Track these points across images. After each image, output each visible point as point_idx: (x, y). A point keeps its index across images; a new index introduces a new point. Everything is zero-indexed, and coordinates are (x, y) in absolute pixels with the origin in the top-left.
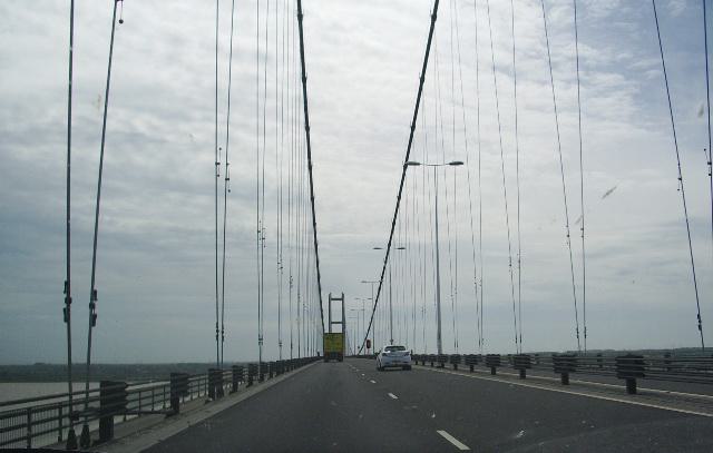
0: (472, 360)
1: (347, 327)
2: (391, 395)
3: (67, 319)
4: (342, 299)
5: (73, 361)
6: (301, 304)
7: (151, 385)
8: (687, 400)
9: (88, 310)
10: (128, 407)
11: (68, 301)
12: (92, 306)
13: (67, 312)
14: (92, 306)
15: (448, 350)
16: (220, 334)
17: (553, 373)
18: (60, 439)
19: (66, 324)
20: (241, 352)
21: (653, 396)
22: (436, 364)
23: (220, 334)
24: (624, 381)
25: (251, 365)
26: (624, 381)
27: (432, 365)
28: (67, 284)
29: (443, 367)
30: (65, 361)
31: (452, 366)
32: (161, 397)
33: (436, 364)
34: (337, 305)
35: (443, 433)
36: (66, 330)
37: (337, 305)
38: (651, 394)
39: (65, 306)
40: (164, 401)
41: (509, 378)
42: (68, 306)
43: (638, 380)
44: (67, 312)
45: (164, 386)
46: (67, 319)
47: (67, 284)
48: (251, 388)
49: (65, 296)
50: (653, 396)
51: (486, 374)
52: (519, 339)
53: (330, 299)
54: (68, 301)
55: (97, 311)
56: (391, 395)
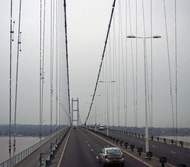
4: (77, 101)
34: (75, 103)
37: (75, 103)
53: (73, 101)
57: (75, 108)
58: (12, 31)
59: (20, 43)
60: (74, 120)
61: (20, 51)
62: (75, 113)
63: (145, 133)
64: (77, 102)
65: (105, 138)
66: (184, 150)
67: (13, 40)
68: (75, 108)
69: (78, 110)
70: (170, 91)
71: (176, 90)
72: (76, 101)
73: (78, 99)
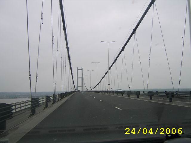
0: (117, 92)
3: (30, 80)
4: (82, 70)
6: (63, 61)
8: (142, 98)
10: (39, 103)
11: (30, 75)
12: (37, 77)
13: (30, 78)
14: (37, 77)
16: (54, 83)
17: (147, 96)
20: (60, 90)
21: (176, 103)
22: (102, 93)
23: (54, 83)
24: (149, 97)
25: (112, 91)
26: (149, 97)
28: (30, 72)
29: (110, 94)
31: (121, 95)
32: (17, 106)
34: (80, 72)
35: (120, 109)
36: (30, 81)
37: (80, 72)
40: (44, 100)
41: (120, 95)
43: (152, 97)
44: (30, 78)
45: (25, 102)
46: (30, 80)
47: (30, 72)
48: (34, 117)
50: (176, 103)
51: (127, 97)
52: (176, 83)
53: (78, 70)
57: (80, 76)
62: (80, 80)
69: (82, 78)
73: (82, 68)
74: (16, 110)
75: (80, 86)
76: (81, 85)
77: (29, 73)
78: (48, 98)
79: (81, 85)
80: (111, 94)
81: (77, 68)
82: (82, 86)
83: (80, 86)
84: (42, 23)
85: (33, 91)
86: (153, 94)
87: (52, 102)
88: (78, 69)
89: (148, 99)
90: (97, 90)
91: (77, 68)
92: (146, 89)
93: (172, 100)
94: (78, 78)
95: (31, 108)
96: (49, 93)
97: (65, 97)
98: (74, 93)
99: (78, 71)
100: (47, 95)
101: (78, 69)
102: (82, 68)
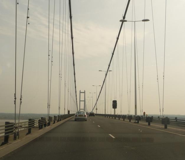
1: (86, 103)
2: (99, 126)
3: (15, 104)
4: (84, 92)
5: (21, 113)
7: (180, 135)
9: (20, 100)
11: (15, 98)
12: (21, 99)
13: (15, 101)
14: (21, 99)
15: (107, 113)
16: (49, 106)
18: (18, 129)
19: (15, 105)
20: (54, 111)
22: (113, 118)
23: (49, 106)
26: (164, 125)
27: (112, 118)
28: (15, 94)
30: (134, 114)
33: (113, 118)
34: (82, 95)
37: (82, 95)
38: (158, 129)
39: (14, 100)
42: (15, 100)
44: (15, 101)
45: (25, 122)
46: (15, 104)
47: (15, 94)
48: (29, 135)
49: (15, 97)
51: (122, 121)
53: (80, 92)
54: (15, 98)
55: (22, 101)
56: (99, 126)
57: (82, 99)
58: (28, 16)
59: (29, 17)
60: (81, 101)
61: (29, 24)
62: (82, 103)
63: (2, 157)
64: (84, 93)
65: (107, 117)
66: (139, 130)
67: (18, 4)
68: (82, 99)
69: (85, 101)
70: (157, 78)
71: (158, 79)
72: (83, 93)
73: (85, 91)
74: (26, 125)
75: (83, 101)
76: (83, 108)
77: (14, 95)
78: (31, 121)
79: (83, 108)
80: (117, 118)
81: (80, 91)
82: (84, 109)
83: (83, 101)
84: (29, 24)
85: (17, 112)
86: (152, 120)
87: (57, 121)
88: (81, 92)
89: (122, 121)
90: (99, 113)
91: (80, 91)
92: (162, 114)
93: (150, 124)
94: (80, 101)
95: (5, 131)
96: (44, 115)
97: (63, 119)
98: (79, 118)
99: (81, 93)
100: (42, 117)
101: (81, 100)
102: (85, 91)
